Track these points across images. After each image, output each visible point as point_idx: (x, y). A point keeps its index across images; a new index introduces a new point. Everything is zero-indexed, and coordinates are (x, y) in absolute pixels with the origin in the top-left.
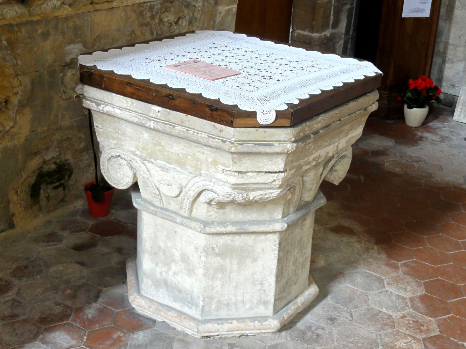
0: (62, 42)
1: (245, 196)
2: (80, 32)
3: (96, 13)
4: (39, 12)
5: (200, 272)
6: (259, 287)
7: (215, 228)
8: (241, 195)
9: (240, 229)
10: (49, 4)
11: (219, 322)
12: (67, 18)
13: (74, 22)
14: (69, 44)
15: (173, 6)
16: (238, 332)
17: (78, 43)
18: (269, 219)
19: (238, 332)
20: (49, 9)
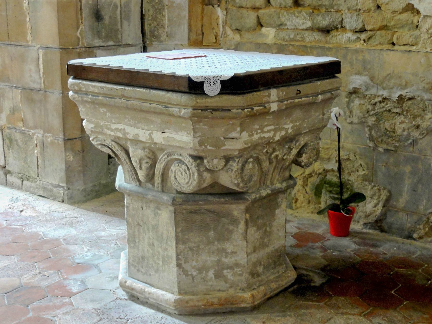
0: (349, 71)
2: (369, 67)
3: (389, 52)
4: (335, 42)
5: (41, 211)
10: (344, 36)
12: (357, 51)
13: (364, 56)
14: (356, 74)
17: (365, 75)
20: (344, 40)
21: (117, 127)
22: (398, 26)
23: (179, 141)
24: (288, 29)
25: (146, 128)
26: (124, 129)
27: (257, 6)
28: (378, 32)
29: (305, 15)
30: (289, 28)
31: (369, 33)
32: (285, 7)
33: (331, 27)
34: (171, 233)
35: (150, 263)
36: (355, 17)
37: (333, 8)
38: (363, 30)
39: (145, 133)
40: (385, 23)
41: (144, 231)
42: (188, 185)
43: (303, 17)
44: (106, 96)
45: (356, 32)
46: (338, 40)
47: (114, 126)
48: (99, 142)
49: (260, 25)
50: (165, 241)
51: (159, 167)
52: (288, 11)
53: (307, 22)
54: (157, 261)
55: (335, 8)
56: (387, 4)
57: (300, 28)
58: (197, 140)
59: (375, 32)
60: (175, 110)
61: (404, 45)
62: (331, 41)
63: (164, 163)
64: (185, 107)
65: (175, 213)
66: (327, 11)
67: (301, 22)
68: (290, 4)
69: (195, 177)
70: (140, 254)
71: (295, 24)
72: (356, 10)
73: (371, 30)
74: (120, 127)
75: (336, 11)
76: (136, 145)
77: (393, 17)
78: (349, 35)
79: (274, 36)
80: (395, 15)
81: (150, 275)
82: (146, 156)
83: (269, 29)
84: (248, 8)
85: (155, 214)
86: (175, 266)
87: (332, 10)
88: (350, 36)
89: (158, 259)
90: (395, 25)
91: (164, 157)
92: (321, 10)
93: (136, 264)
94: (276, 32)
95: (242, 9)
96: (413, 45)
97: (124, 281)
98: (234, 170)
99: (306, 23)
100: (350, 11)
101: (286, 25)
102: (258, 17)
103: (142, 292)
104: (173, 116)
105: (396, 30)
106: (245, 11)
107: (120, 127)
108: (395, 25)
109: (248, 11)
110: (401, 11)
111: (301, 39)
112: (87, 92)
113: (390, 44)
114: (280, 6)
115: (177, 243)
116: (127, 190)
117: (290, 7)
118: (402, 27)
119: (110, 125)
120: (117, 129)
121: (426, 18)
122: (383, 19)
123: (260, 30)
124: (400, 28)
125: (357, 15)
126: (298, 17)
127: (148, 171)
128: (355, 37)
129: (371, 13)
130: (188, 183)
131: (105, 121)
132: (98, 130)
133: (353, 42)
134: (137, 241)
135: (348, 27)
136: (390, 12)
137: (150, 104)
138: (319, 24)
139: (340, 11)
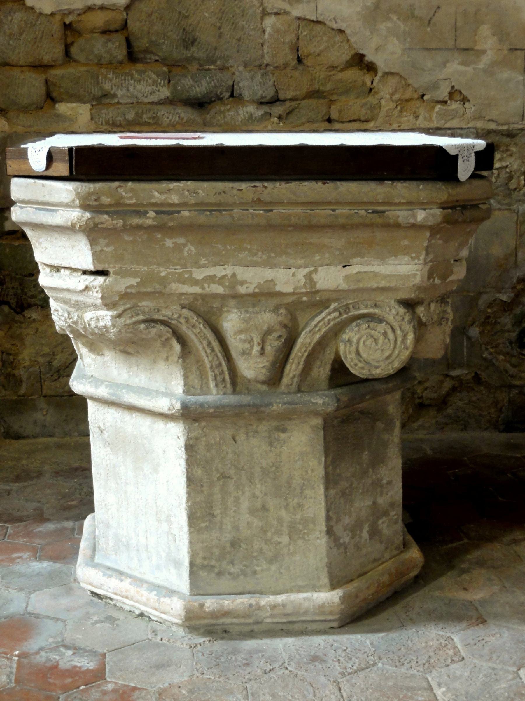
1: (75, 318)
4: (221, 122)
6: (165, 526)
7: (84, 385)
8: (66, 315)
9: (113, 394)
10: (241, 112)
11: (109, 572)
15: (516, 144)
16: (157, 613)
18: (164, 391)
19: (157, 613)
21: (211, 274)
22: (339, 91)
23: (386, 277)
24: (118, 103)
25: (301, 262)
26: (234, 275)
27: (45, 62)
28: (304, 103)
29: (154, 76)
30: (121, 101)
31: (288, 104)
32: (110, 63)
33: (211, 98)
34: (313, 471)
35: (256, 547)
36: (258, 77)
37: (214, 62)
38: (275, 100)
39: (294, 275)
40: (316, 86)
41: (237, 488)
42: (389, 361)
43: (150, 81)
44: (201, 206)
45: (261, 103)
46: (228, 119)
47: (199, 274)
48: (141, 317)
49: (51, 98)
50: (298, 491)
51: (308, 340)
52: (117, 71)
53: (161, 89)
54: (276, 539)
55: (219, 63)
56: (319, 55)
57: (146, 100)
58: (427, 267)
59: (298, 102)
60: (402, 215)
61: (350, 121)
62: (215, 121)
63: (323, 330)
64: (423, 205)
65: (324, 429)
66: (202, 69)
67: (149, 89)
68: (120, 58)
69: (409, 341)
70: (227, 537)
71: (136, 93)
72: (260, 66)
73: (291, 100)
74: (219, 271)
75: (220, 69)
76: (254, 306)
77: (331, 76)
78: (251, 109)
79: (89, 118)
80: (333, 73)
81: (255, 572)
82: (281, 323)
83: (74, 105)
84: (21, 66)
85: (271, 444)
86: (324, 534)
87: (212, 67)
88: (253, 111)
89: (279, 532)
90: (334, 90)
91: (329, 317)
92: (190, 68)
93: (213, 563)
94: (91, 110)
95: (7, 68)
96: (367, 121)
97: (196, 604)
98: (451, 319)
99: (159, 91)
100: (248, 69)
101: (115, 96)
102: (46, 81)
103: (250, 611)
104: (397, 226)
105: (335, 97)
106: (16, 72)
107: (219, 271)
108: (334, 90)
109: (22, 72)
110: (342, 66)
111: (151, 121)
112: (142, 205)
113: (324, 121)
114: (100, 60)
115: (327, 489)
116: (209, 407)
117: (121, 63)
118: (347, 92)
119: (191, 272)
120: (211, 279)
121: (386, 76)
122: (312, 80)
123: (53, 107)
124: (341, 94)
125: (262, 75)
126: (139, 81)
127: (277, 354)
128: (260, 112)
129: (288, 70)
130: (388, 358)
131: (177, 264)
132: (149, 290)
133: (258, 121)
134: (217, 512)
135: (246, 95)
136: (324, 69)
137: (334, 210)
138: (188, 91)
139: (228, 68)
